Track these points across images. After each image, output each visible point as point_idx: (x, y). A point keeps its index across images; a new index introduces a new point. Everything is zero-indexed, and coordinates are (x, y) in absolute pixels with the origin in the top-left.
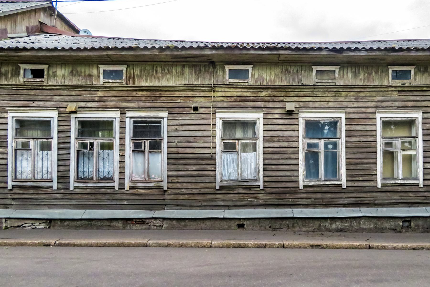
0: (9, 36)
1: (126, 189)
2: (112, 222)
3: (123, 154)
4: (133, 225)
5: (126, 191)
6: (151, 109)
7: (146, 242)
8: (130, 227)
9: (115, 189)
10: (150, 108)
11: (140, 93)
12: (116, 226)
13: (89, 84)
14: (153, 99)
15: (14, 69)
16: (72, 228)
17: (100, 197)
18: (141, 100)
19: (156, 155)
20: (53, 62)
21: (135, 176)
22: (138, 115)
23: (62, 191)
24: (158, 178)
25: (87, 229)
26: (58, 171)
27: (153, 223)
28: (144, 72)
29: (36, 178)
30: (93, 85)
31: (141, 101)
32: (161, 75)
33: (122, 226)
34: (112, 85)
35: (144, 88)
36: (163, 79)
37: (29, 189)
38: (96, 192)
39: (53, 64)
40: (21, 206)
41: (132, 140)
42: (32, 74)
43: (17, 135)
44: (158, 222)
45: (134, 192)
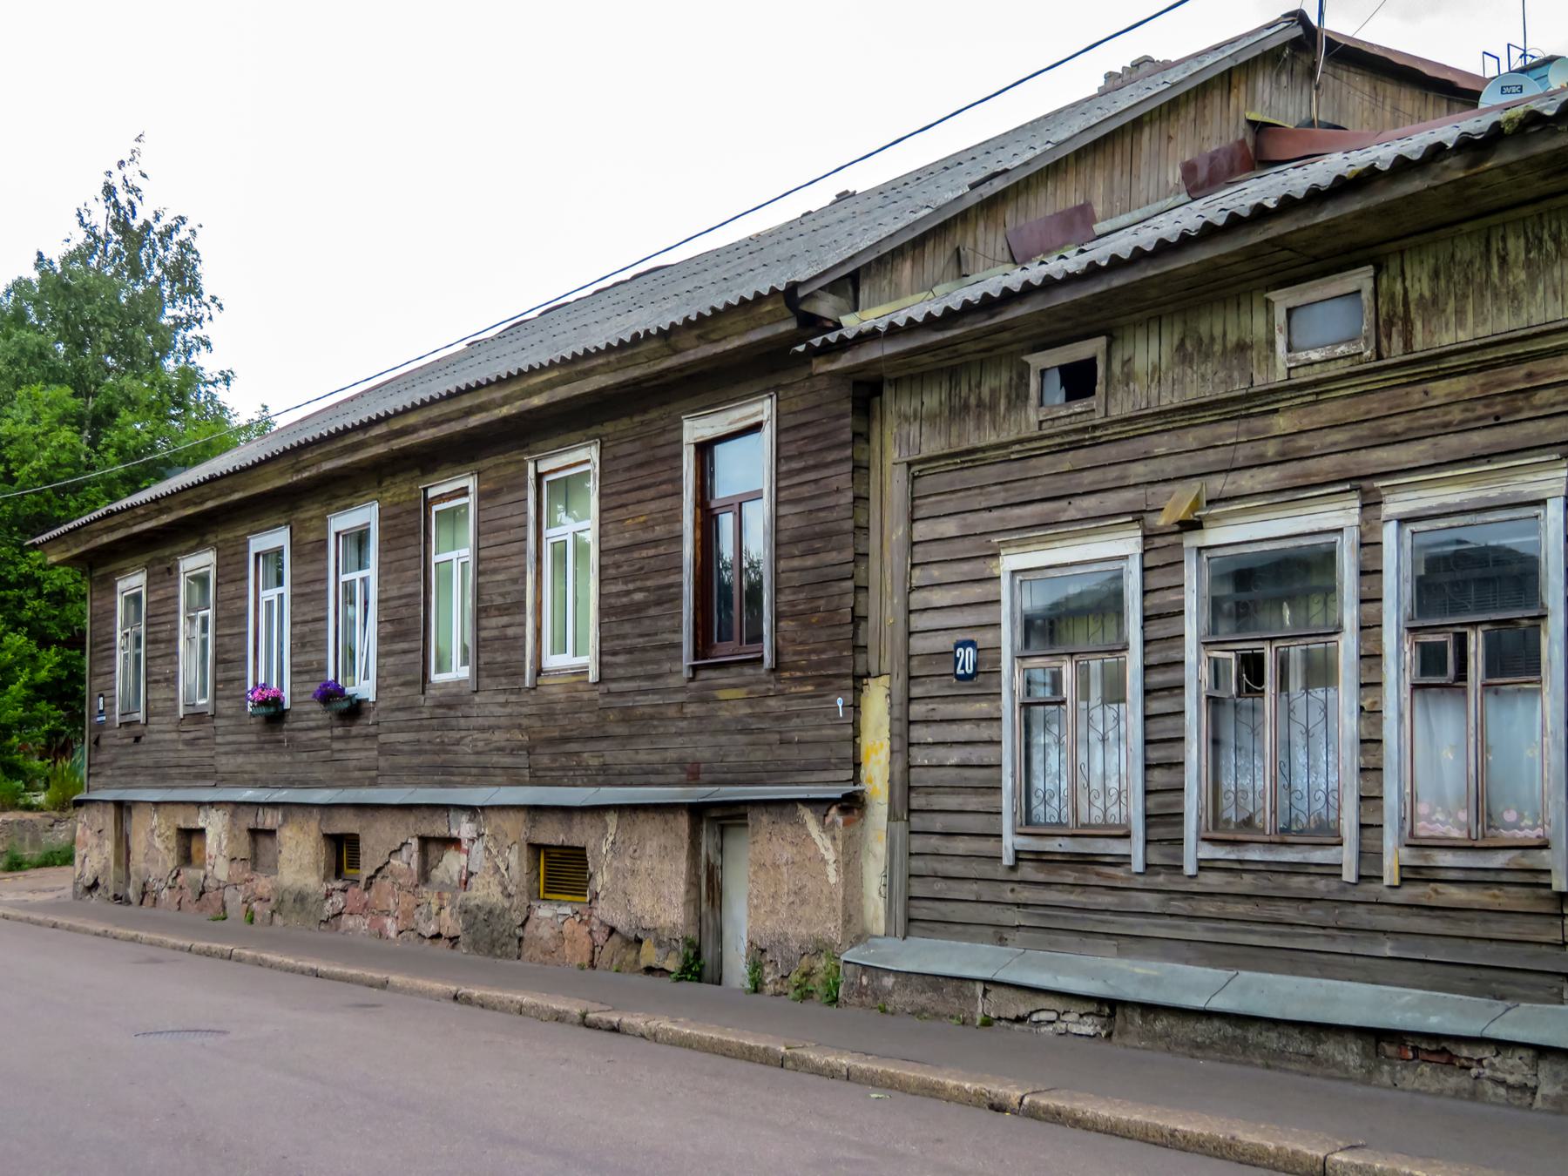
0: (1099, 228)
1: (1387, 882)
2: (1320, 1042)
3: (1375, 703)
4: (1406, 1067)
5: (1387, 891)
6: (1495, 459)
7: (1321, 1155)
8: (1392, 1075)
9: (1345, 878)
10: (1488, 457)
11: (1441, 390)
12: (1336, 1065)
13: (1239, 388)
14: (1498, 408)
15: (1015, 377)
16: (1180, 1050)
17: (1288, 912)
18: (1447, 425)
19: (1520, 707)
20: (1123, 320)
21: (1434, 812)
22: (1434, 502)
23: (1161, 879)
24: (1533, 828)
25: (1231, 1061)
26: (1147, 792)
27: (1492, 1065)
28: (1449, 278)
29: (1083, 818)
30: (1251, 391)
31: (1446, 429)
32: (1523, 276)
33: (1361, 1066)
34: (1322, 372)
35: (1454, 361)
36: (1533, 291)
37: (1062, 868)
38: (1274, 888)
39: (1122, 327)
40: (1038, 935)
41: (1411, 630)
42: (1064, 383)
43: (1034, 643)
44: (1515, 1068)
45: (1424, 895)
